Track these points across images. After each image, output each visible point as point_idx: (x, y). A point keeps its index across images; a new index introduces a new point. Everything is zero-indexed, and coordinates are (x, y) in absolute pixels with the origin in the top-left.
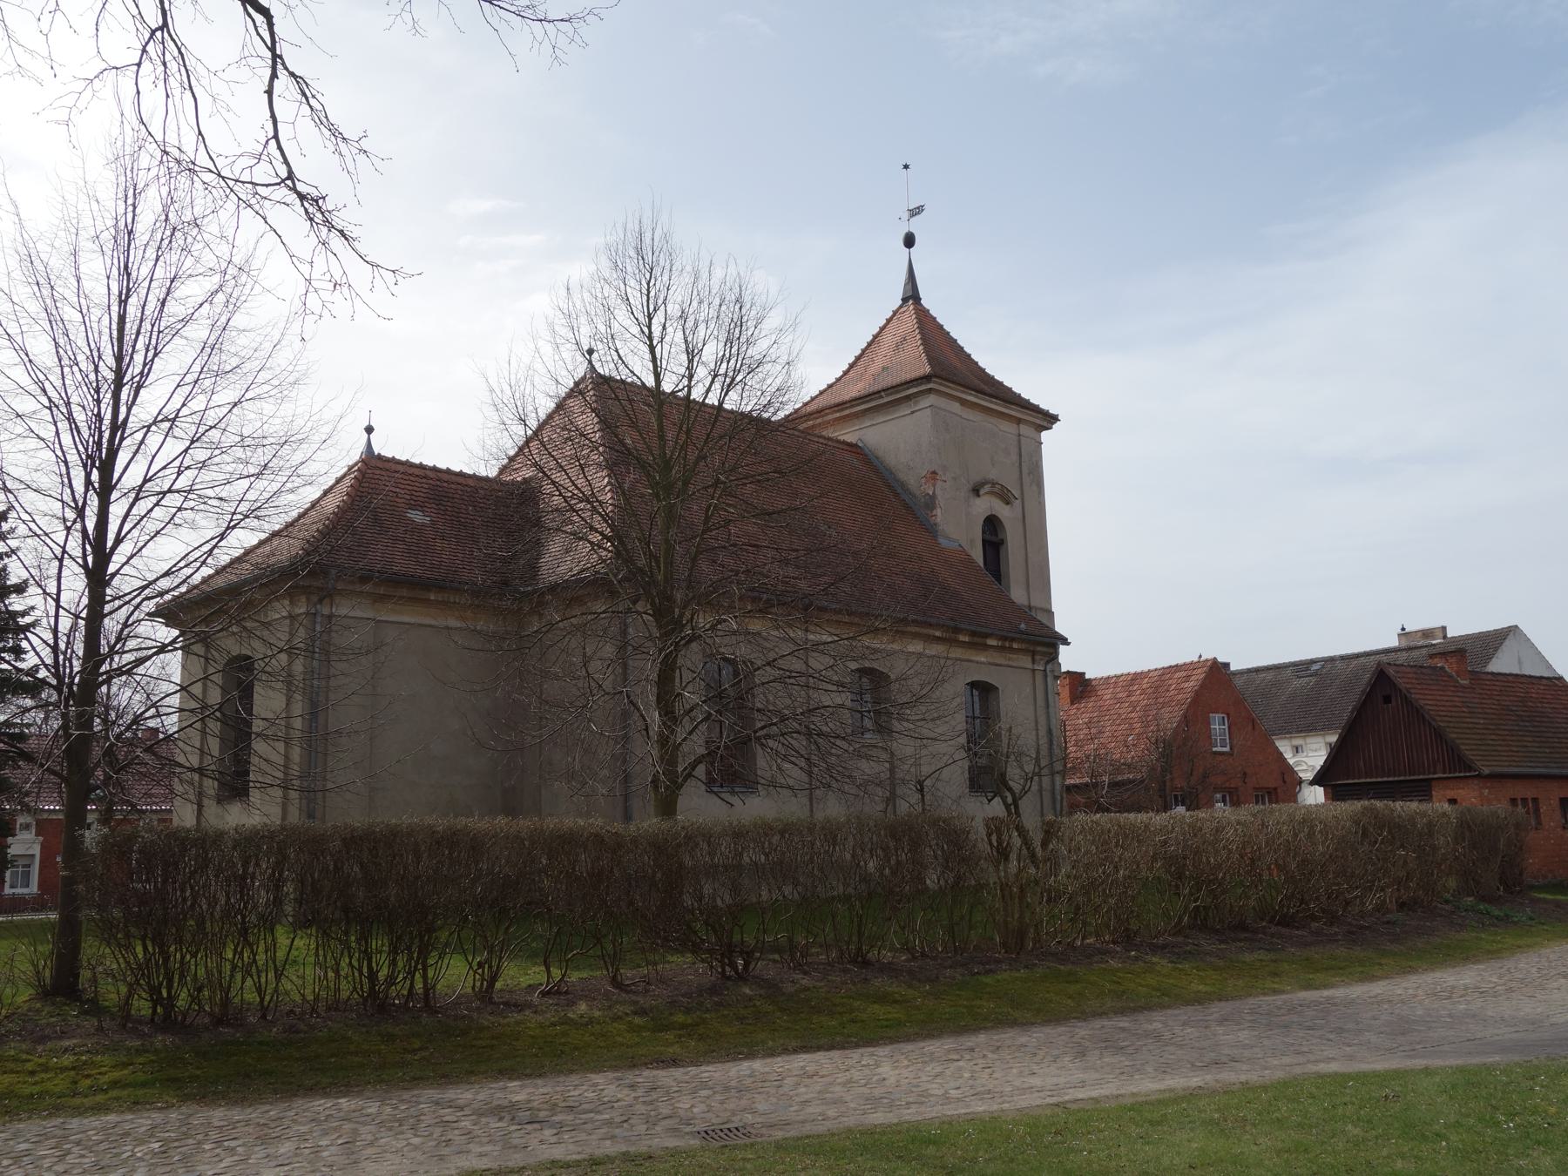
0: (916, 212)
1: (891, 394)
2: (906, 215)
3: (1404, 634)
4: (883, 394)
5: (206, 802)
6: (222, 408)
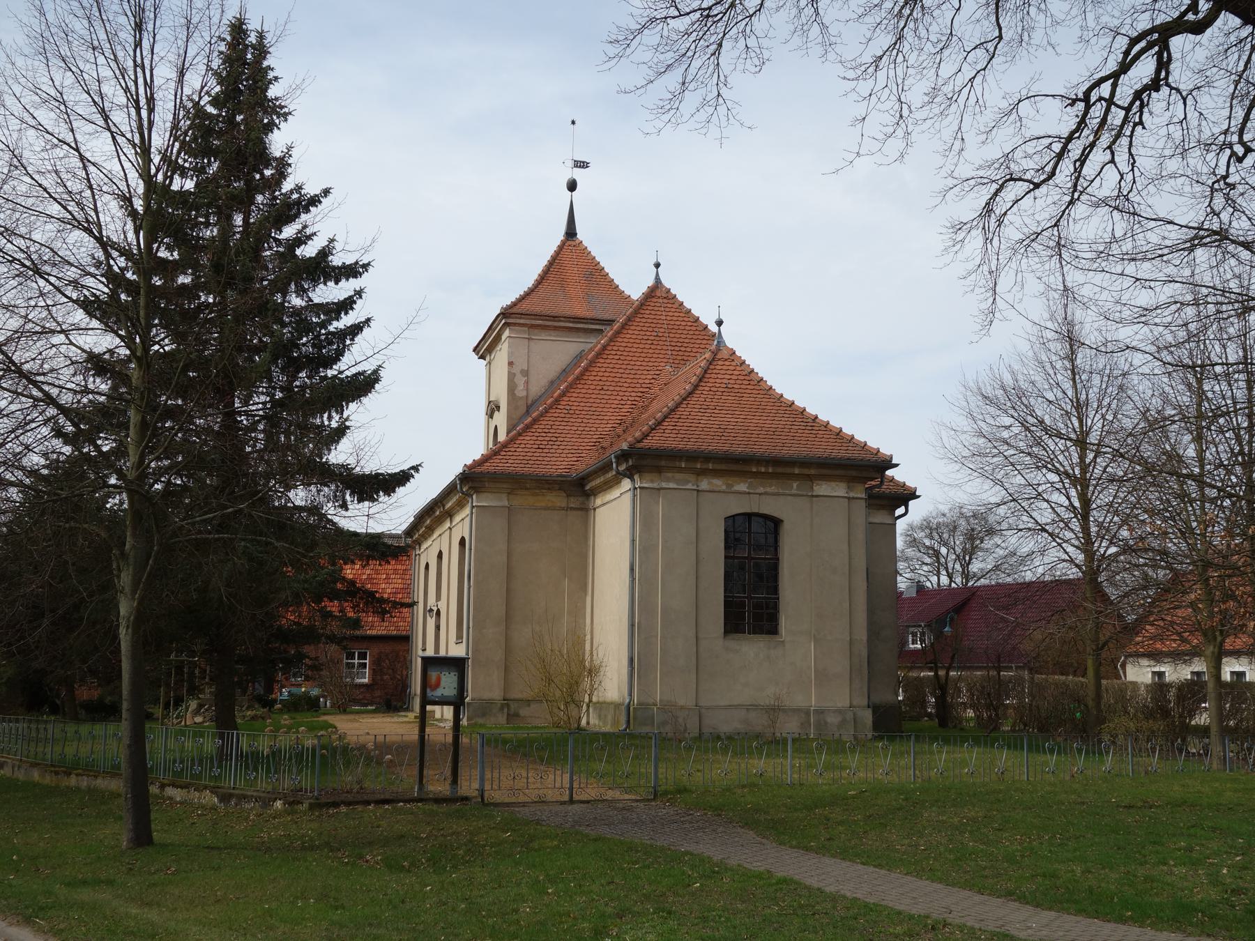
0: (581, 165)
2: (571, 164)
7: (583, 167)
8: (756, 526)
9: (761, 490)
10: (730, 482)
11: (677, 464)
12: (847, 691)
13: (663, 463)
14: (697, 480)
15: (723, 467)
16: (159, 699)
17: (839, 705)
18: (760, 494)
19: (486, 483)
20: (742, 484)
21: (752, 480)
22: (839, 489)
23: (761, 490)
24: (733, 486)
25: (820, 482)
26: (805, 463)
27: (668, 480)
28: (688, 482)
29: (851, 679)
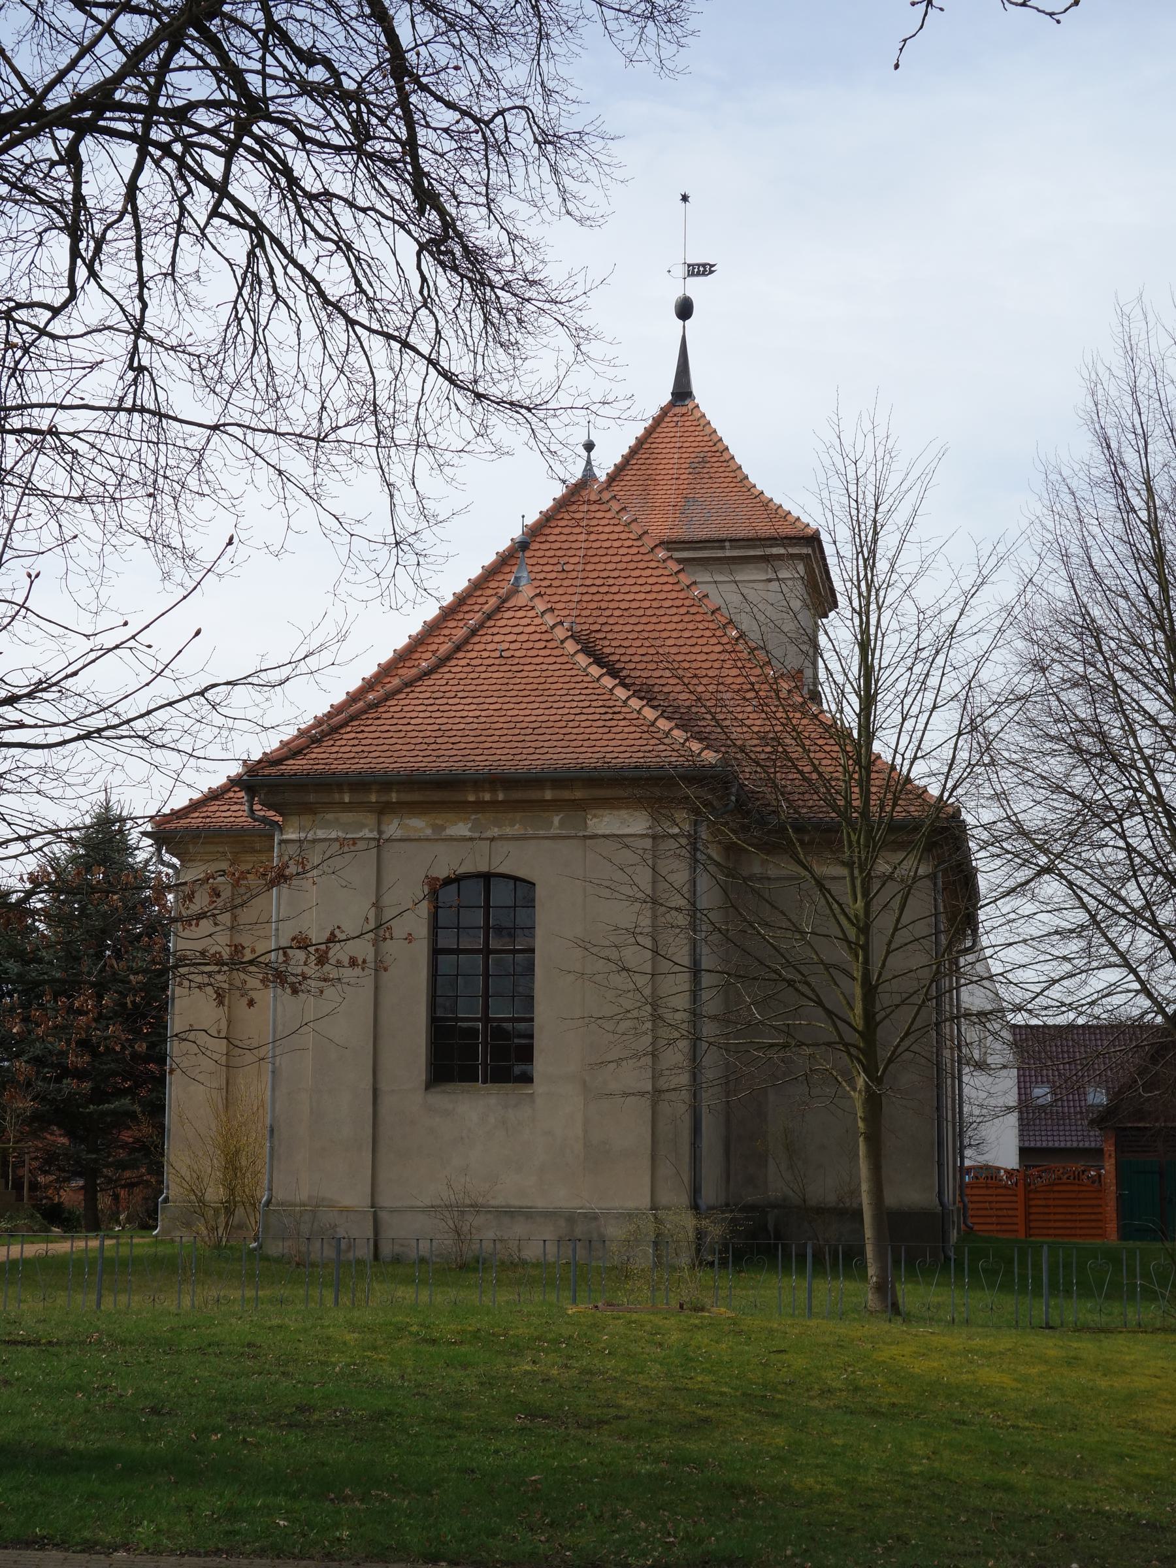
0: (701, 270)
1: (740, 548)
2: (681, 271)
3: (332, 706)
4: (727, 544)
5: (476, 10)
6: (94, 321)
7: (704, 274)
8: (501, 895)
9: (495, 832)
10: (439, 822)
11: (337, 797)
12: (647, 1179)
13: (312, 798)
14: (379, 823)
15: (416, 797)
16: (862, 1252)
17: (630, 1204)
18: (492, 839)
19: (191, 847)
20: (461, 824)
21: (479, 816)
22: (635, 823)
23: (495, 832)
24: (445, 829)
25: (599, 812)
26: (561, 779)
27: (327, 825)
28: (362, 826)
29: (654, 1158)
